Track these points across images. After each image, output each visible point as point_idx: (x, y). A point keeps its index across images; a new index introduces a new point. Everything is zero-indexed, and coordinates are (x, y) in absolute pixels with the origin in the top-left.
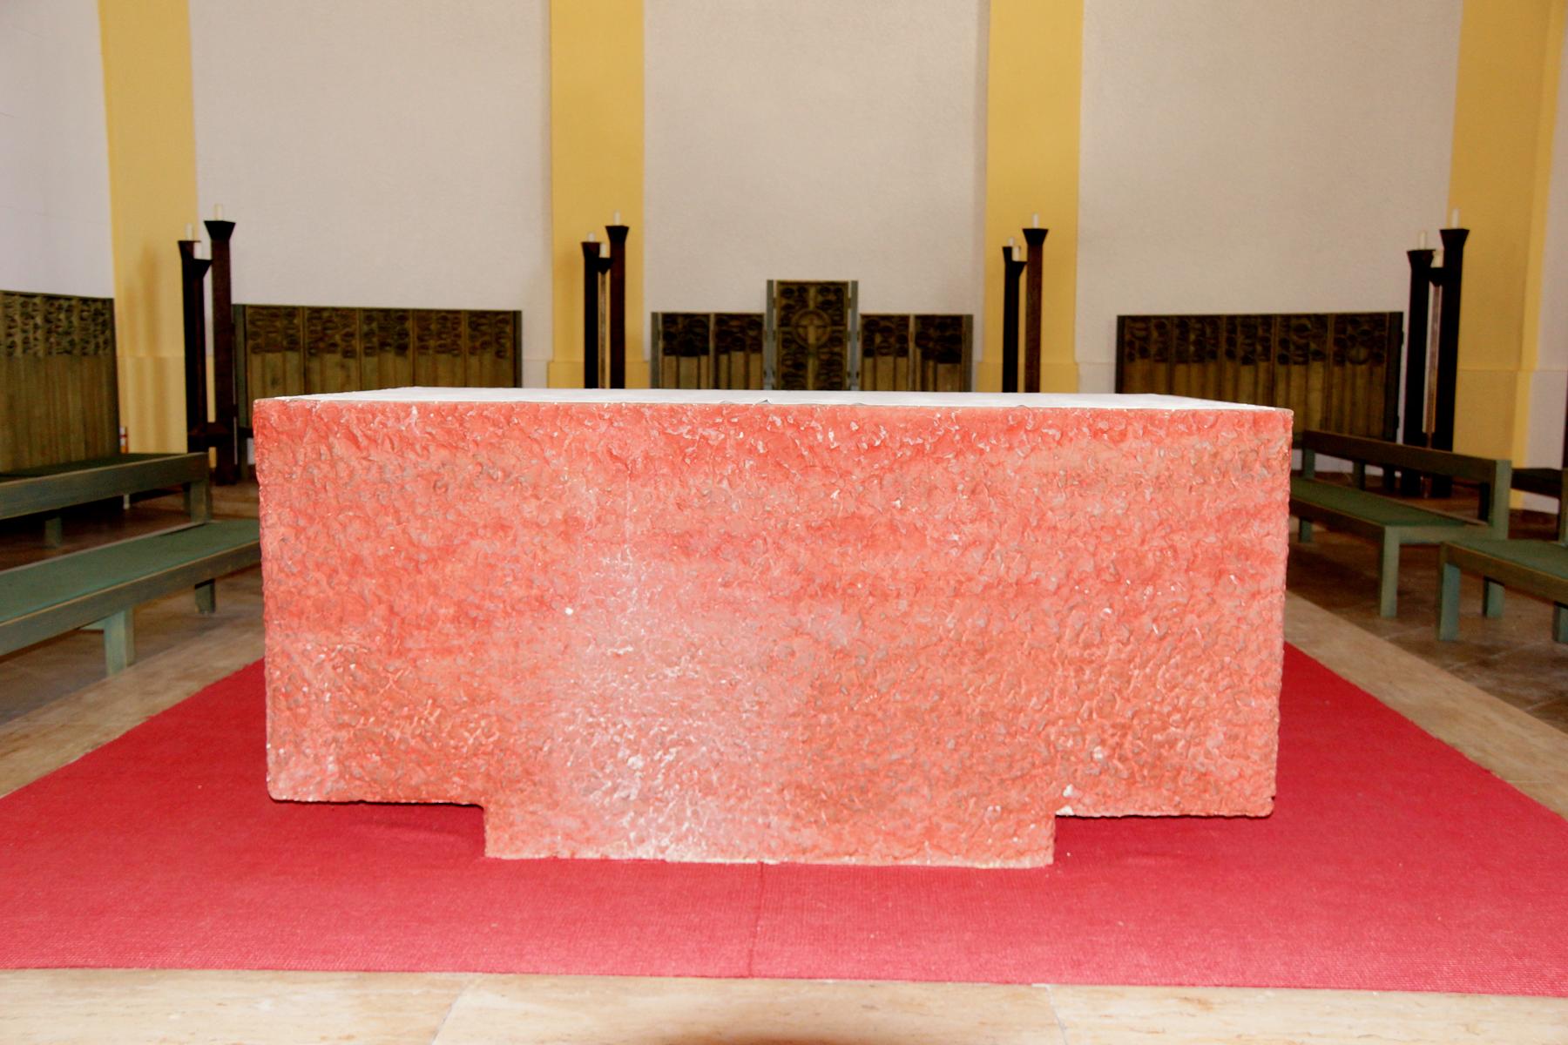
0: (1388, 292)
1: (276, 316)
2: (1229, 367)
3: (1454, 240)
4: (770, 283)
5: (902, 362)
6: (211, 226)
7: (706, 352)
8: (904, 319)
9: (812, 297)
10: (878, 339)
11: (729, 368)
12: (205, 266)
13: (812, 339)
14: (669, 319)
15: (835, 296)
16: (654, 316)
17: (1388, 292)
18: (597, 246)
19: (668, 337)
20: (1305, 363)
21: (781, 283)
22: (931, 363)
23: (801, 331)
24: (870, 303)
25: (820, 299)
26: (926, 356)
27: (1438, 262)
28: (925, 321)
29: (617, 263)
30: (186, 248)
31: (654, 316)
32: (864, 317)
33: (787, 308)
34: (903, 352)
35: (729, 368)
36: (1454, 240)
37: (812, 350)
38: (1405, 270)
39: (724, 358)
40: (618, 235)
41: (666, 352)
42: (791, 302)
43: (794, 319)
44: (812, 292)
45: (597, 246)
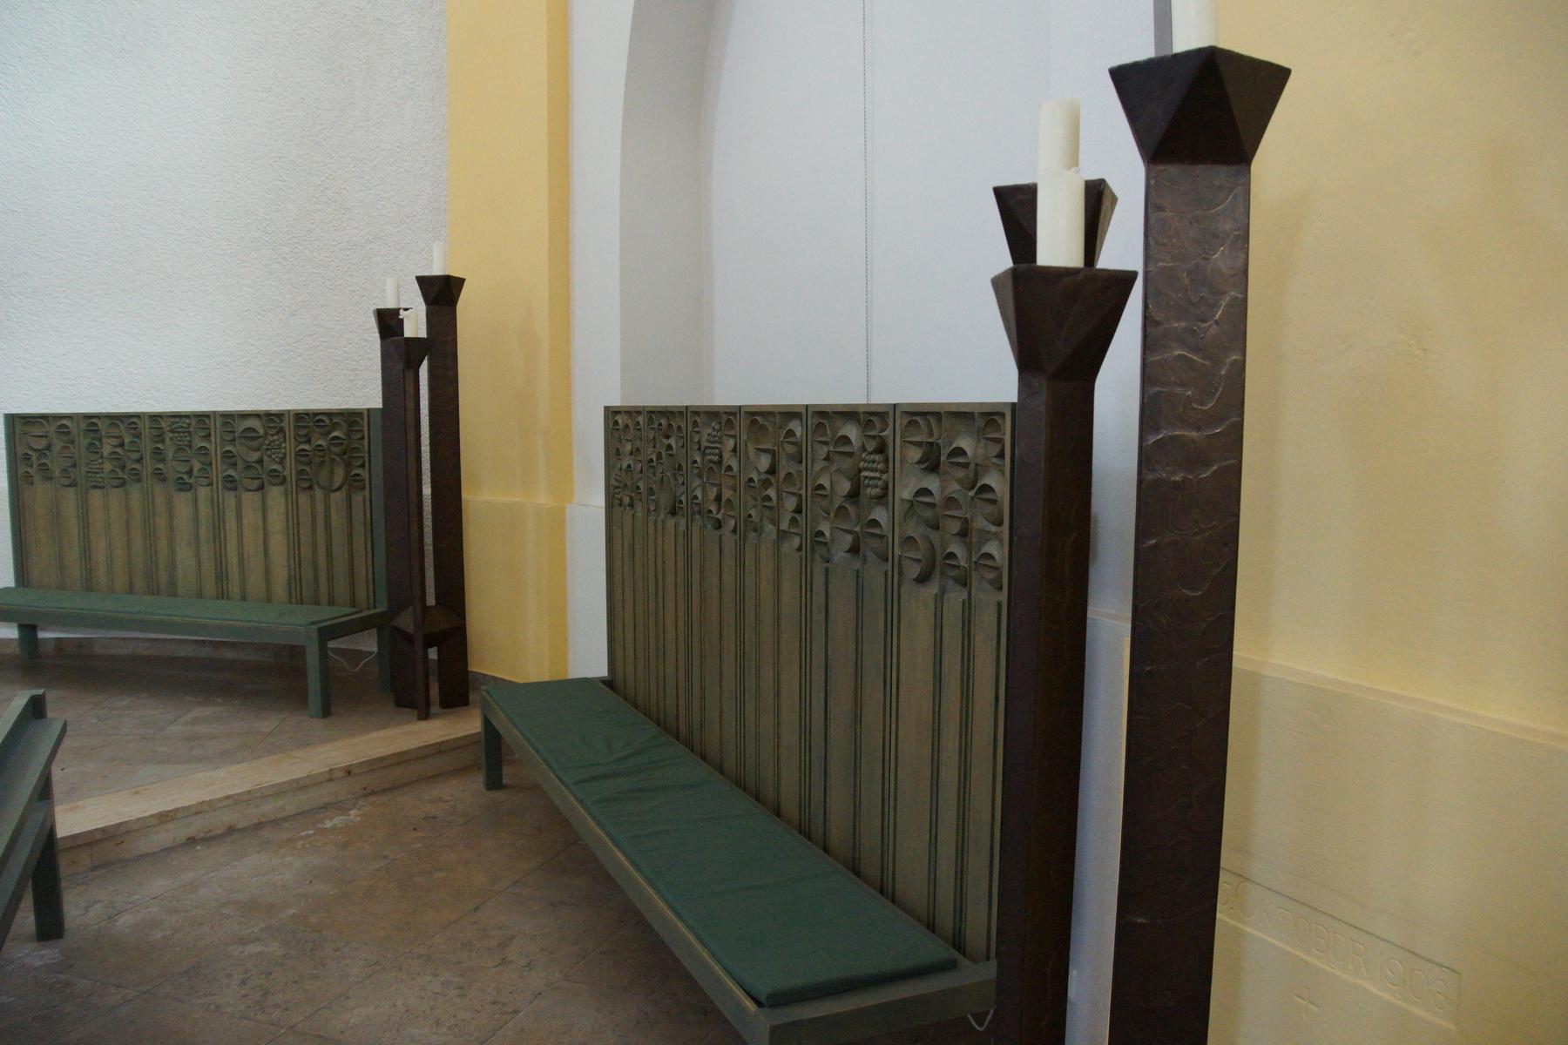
0: (361, 388)
2: (159, 490)
3: (442, 293)
17: (361, 388)
30: (389, 322)
36: (442, 293)
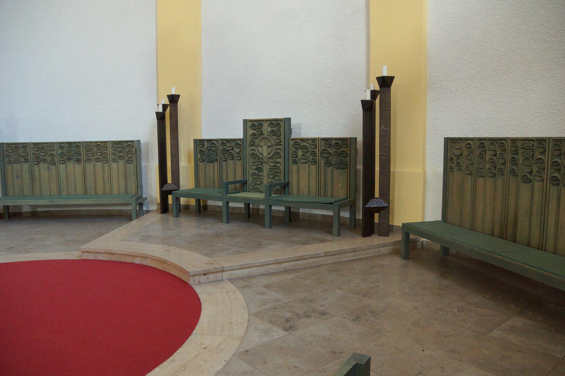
1: (38, 160)
9: (266, 129)
10: (300, 153)
12: (168, 117)
13: (265, 154)
15: (280, 126)
19: (202, 152)
25: (269, 129)
26: (328, 164)
28: (327, 140)
39: (224, 164)
43: (257, 142)
44: (265, 125)
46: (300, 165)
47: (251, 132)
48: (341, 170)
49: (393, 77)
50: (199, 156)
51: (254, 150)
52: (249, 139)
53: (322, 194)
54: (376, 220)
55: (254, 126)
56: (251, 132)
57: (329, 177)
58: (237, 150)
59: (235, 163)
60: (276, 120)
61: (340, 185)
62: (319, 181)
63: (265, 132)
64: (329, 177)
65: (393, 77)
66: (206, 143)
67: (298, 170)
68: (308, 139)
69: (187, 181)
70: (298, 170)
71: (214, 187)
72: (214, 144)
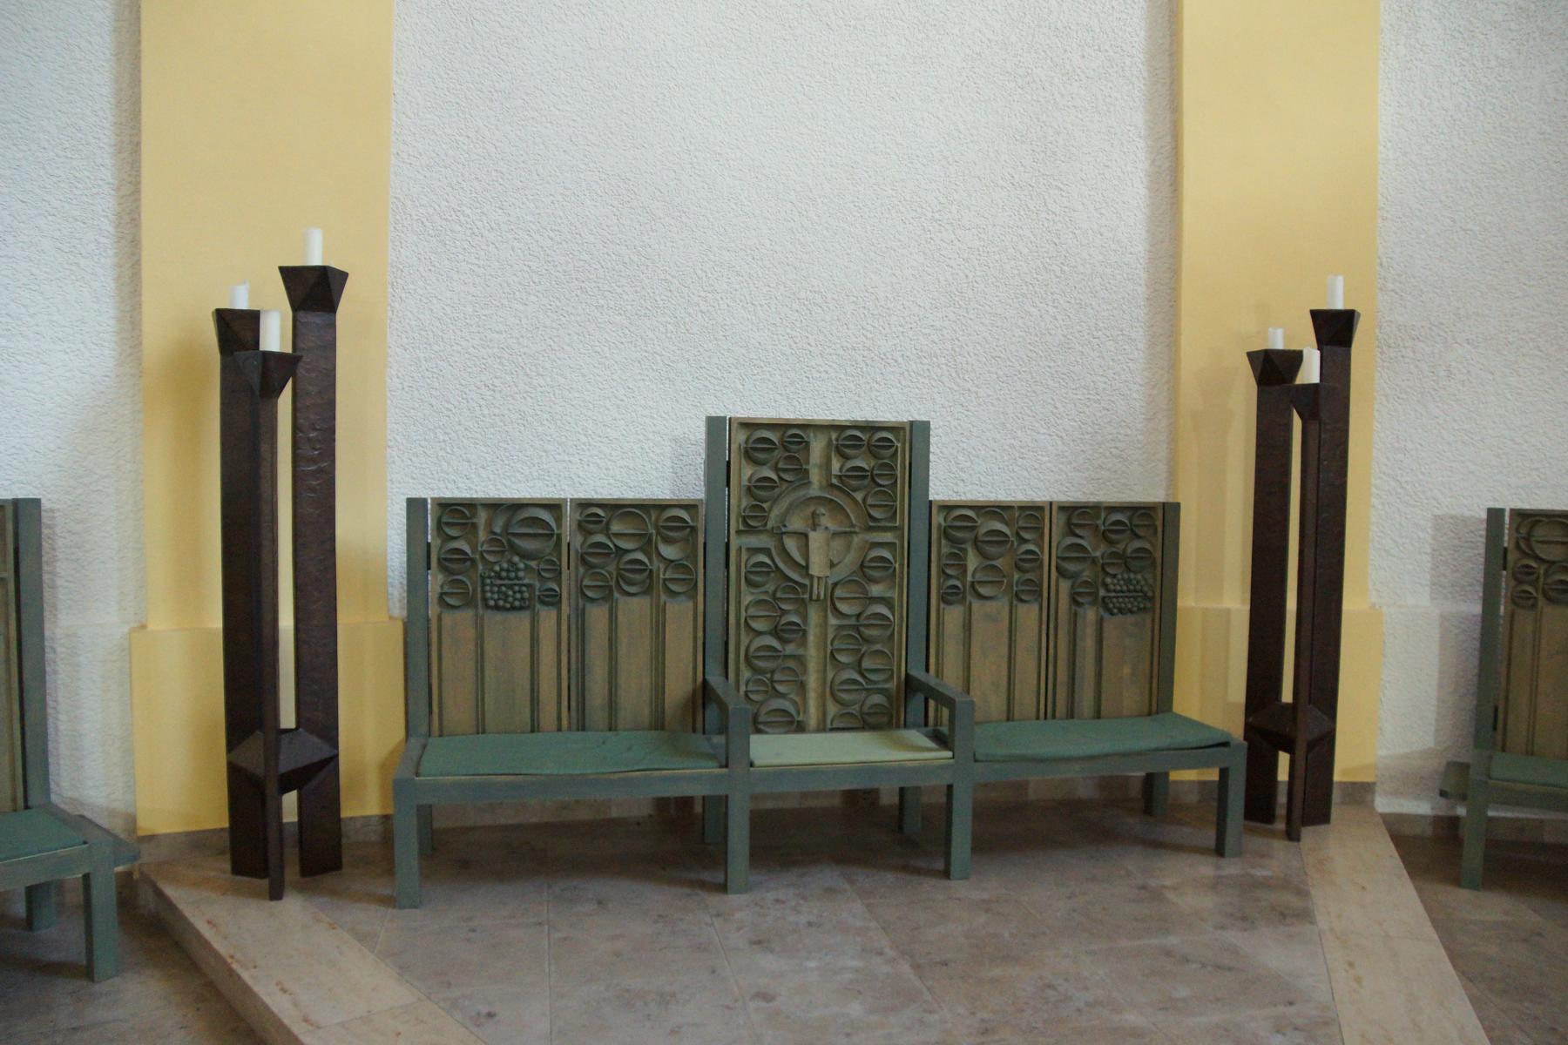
4: (715, 426)
5: (1029, 615)
6: (291, 276)
7: (552, 599)
8: (1032, 513)
11: (612, 642)
13: (817, 567)
14: (456, 513)
15: (880, 458)
16: (415, 506)
18: (251, 319)
19: (452, 563)
20: (608, 597)
21: (749, 425)
22: (1090, 614)
23: (791, 544)
24: (957, 475)
27: (1310, 372)
28: (1077, 515)
29: (309, 370)
31: (415, 506)
32: (947, 508)
33: (757, 489)
34: (1032, 590)
35: (612, 642)
37: (819, 590)
38: (1244, 392)
39: (597, 616)
40: (315, 290)
41: (458, 596)
42: (768, 472)
44: (817, 446)
45: (251, 319)
46: (976, 605)
47: (745, 472)
48: (1130, 619)
49: (283, 270)
50: (435, 581)
51: (766, 551)
52: (738, 501)
53: (1061, 707)
54: (1283, 775)
55: (766, 456)
56: (745, 472)
57: (1088, 644)
58: (669, 551)
59: (660, 611)
60: (871, 428)
61: (1127, 670)
62: (1047, 662)
63: (815, 476)
64: (1088, 644)
65: (283, 270)
66: (482, 517)
67: (968, 626)
68: (1007, 508)
69: (370, 721)
70: (968, 626)
71: (559, 729)
72: (535, 521)
